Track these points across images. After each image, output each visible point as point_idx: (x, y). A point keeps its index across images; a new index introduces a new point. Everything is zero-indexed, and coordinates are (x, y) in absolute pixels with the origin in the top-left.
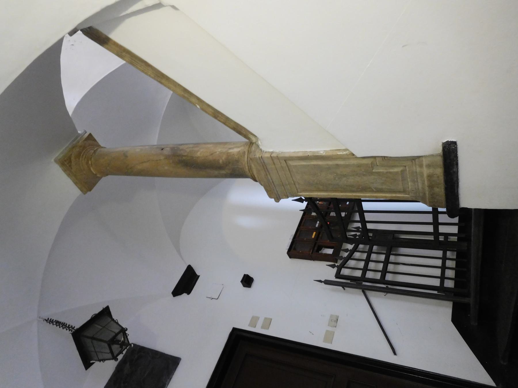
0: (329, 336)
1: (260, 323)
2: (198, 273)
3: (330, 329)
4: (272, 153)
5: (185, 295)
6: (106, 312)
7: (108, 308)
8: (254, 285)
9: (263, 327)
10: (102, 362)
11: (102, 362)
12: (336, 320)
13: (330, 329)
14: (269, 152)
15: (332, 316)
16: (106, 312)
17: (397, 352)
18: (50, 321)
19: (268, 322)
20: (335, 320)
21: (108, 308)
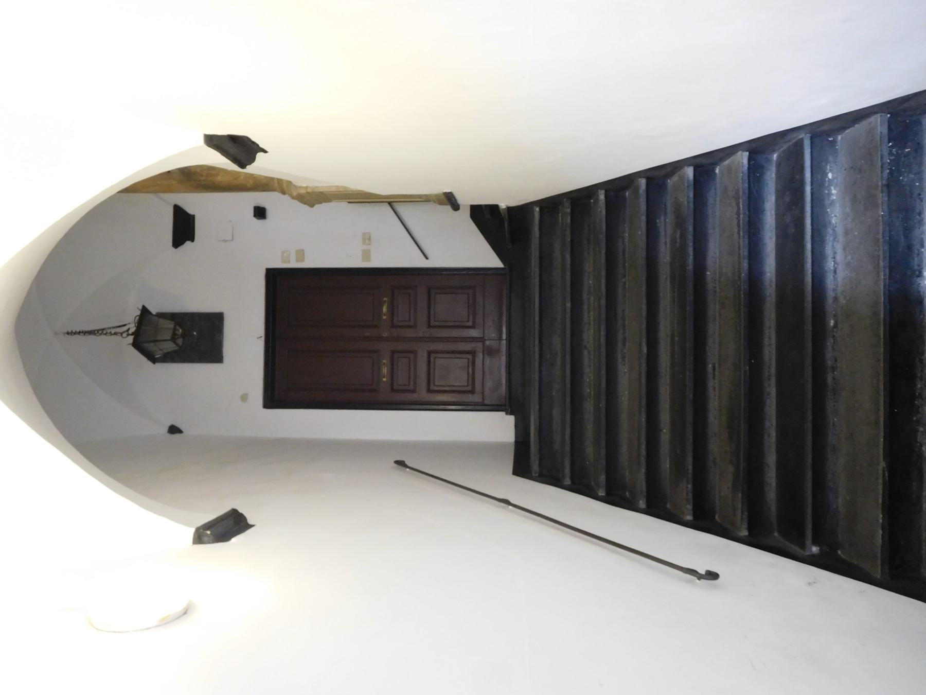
0: (366, 255)
1: (293, 257)
2: (190, 212)
3: (365, 247)
4: (307, 187)
5: (188, 243)
6: (145, 311)
7: (144, 307)
8: (269, 213)
9: (298, 260)
10: (74, 331)
11: (74, 331)
12: (369, 237)
13: (365, 247)
14: (304, 187)
15: (364, 234)
16: (145, 311)
17: (429, 256)
18: (68, 333)
19: (301, 255)
20: (367, 238)
21: (144, 307)
